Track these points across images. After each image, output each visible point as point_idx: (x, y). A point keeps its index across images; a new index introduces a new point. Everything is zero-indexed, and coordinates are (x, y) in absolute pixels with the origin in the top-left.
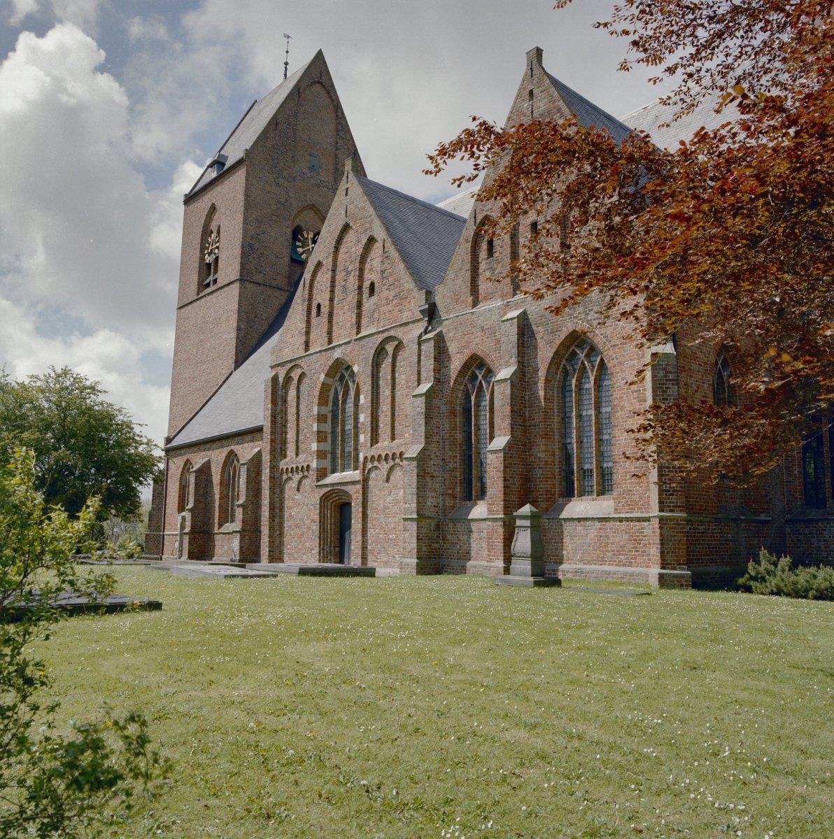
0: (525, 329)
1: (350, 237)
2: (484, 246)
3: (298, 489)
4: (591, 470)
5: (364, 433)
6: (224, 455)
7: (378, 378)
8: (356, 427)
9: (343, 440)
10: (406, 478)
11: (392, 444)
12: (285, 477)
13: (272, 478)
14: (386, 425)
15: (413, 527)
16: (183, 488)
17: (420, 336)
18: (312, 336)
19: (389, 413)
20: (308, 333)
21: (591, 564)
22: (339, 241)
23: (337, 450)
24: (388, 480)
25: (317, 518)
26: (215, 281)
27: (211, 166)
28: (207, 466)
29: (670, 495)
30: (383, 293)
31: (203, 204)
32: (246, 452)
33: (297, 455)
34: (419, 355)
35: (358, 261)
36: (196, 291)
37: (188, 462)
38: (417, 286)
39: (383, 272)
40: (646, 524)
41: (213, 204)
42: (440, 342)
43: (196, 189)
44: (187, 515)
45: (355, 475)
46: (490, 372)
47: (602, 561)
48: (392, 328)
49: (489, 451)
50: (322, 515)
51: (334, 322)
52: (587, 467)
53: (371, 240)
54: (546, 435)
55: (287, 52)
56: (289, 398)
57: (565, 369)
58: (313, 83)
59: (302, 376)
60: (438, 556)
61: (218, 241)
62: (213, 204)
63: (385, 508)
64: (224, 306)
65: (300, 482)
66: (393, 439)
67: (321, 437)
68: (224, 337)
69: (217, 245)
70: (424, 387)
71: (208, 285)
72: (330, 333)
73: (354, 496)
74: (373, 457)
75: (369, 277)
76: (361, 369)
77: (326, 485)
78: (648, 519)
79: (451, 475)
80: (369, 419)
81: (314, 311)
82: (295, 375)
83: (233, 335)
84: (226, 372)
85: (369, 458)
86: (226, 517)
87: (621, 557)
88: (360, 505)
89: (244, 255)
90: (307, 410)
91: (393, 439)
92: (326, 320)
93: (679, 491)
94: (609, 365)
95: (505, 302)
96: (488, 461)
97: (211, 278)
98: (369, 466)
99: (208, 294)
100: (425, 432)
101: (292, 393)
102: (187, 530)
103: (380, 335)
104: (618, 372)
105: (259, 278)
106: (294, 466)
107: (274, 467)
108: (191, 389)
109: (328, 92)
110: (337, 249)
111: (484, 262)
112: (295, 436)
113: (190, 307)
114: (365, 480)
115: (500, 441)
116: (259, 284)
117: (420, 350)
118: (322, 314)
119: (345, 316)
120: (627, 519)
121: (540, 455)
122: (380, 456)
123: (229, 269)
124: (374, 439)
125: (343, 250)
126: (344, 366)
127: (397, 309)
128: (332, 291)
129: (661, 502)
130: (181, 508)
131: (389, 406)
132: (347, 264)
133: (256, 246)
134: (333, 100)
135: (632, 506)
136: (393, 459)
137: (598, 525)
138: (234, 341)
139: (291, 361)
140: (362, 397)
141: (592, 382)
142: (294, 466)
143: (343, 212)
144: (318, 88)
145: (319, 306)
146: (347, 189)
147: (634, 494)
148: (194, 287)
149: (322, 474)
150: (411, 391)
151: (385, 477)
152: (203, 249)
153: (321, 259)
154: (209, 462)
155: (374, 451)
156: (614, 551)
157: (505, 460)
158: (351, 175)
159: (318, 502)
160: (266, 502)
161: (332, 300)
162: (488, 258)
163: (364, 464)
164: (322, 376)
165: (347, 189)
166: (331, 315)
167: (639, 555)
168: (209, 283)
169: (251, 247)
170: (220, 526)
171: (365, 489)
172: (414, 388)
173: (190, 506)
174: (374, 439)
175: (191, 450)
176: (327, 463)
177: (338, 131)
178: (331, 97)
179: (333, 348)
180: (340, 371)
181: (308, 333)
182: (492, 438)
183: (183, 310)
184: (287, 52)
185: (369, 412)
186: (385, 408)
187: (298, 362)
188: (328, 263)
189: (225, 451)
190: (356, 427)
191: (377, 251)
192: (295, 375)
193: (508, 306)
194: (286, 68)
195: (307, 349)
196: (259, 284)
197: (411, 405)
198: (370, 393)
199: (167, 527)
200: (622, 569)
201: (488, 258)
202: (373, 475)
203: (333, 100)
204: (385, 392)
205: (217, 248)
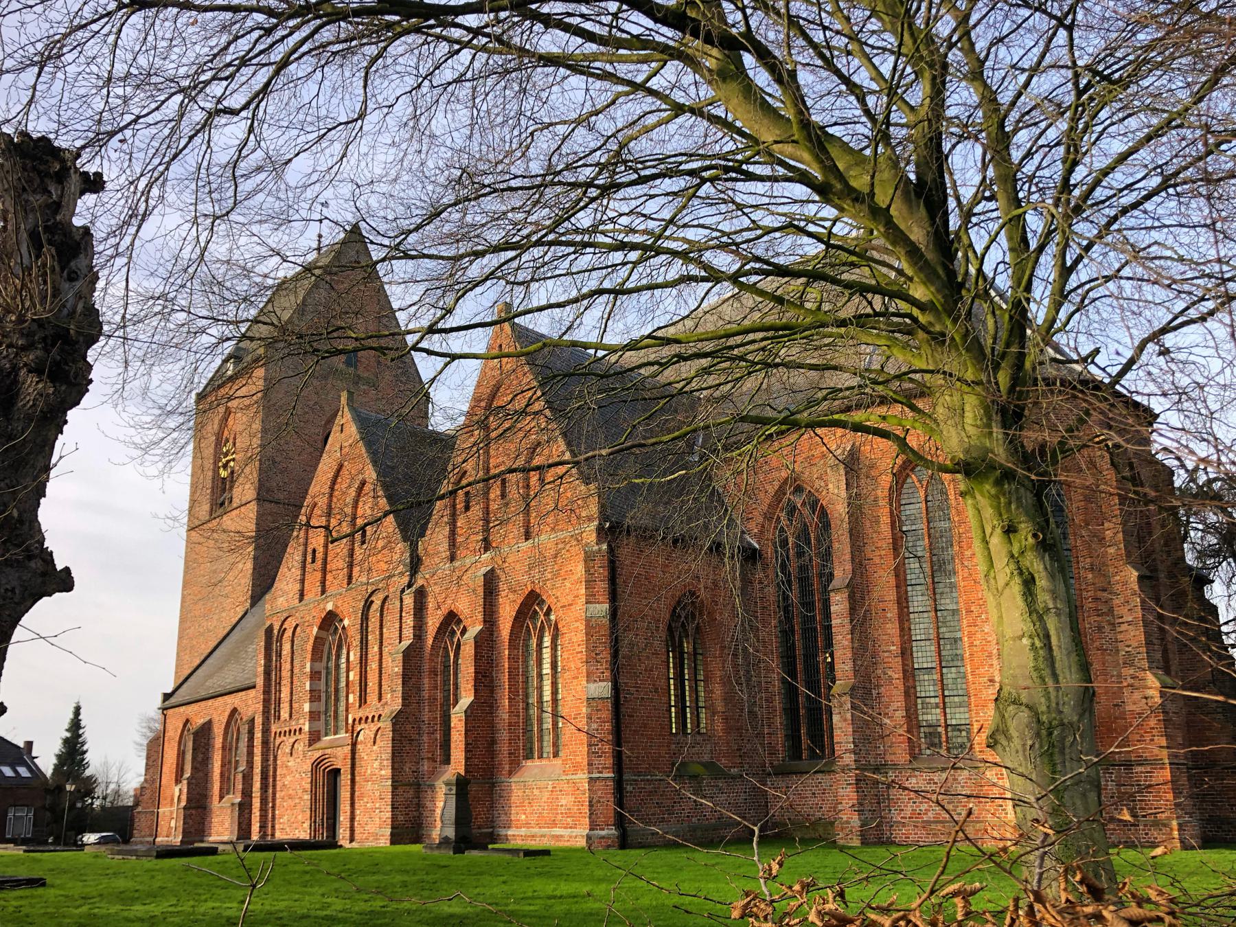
16: (181, 755)
20: (303, 581)
23: (326, 711)
25: (309, 786)
34: (401, 611)
47: (554, 824)
50: (314, 783)
56: (284, 653)
64: (243, 518)
67: (314, 696)
70: (406, 643)
72: (323, 582)
76: (349, 622)
80: (358, 678)
81: (309, 559)
82: (290, 625)
102: (183, 804)
107: (266, 731)
124: (363, 700)
130: (178, 781)
140: (351, 654)
145: (314, 551)
155: (361, 714)
160: (257, 770)
164: (315, 629)
173: (187, 775)
174: (363, 700)
180: (330, 621)
181: (303, 581)
186: (373, 665)
192: (290, 625)
202: (361, 738)
204: (374, 649)
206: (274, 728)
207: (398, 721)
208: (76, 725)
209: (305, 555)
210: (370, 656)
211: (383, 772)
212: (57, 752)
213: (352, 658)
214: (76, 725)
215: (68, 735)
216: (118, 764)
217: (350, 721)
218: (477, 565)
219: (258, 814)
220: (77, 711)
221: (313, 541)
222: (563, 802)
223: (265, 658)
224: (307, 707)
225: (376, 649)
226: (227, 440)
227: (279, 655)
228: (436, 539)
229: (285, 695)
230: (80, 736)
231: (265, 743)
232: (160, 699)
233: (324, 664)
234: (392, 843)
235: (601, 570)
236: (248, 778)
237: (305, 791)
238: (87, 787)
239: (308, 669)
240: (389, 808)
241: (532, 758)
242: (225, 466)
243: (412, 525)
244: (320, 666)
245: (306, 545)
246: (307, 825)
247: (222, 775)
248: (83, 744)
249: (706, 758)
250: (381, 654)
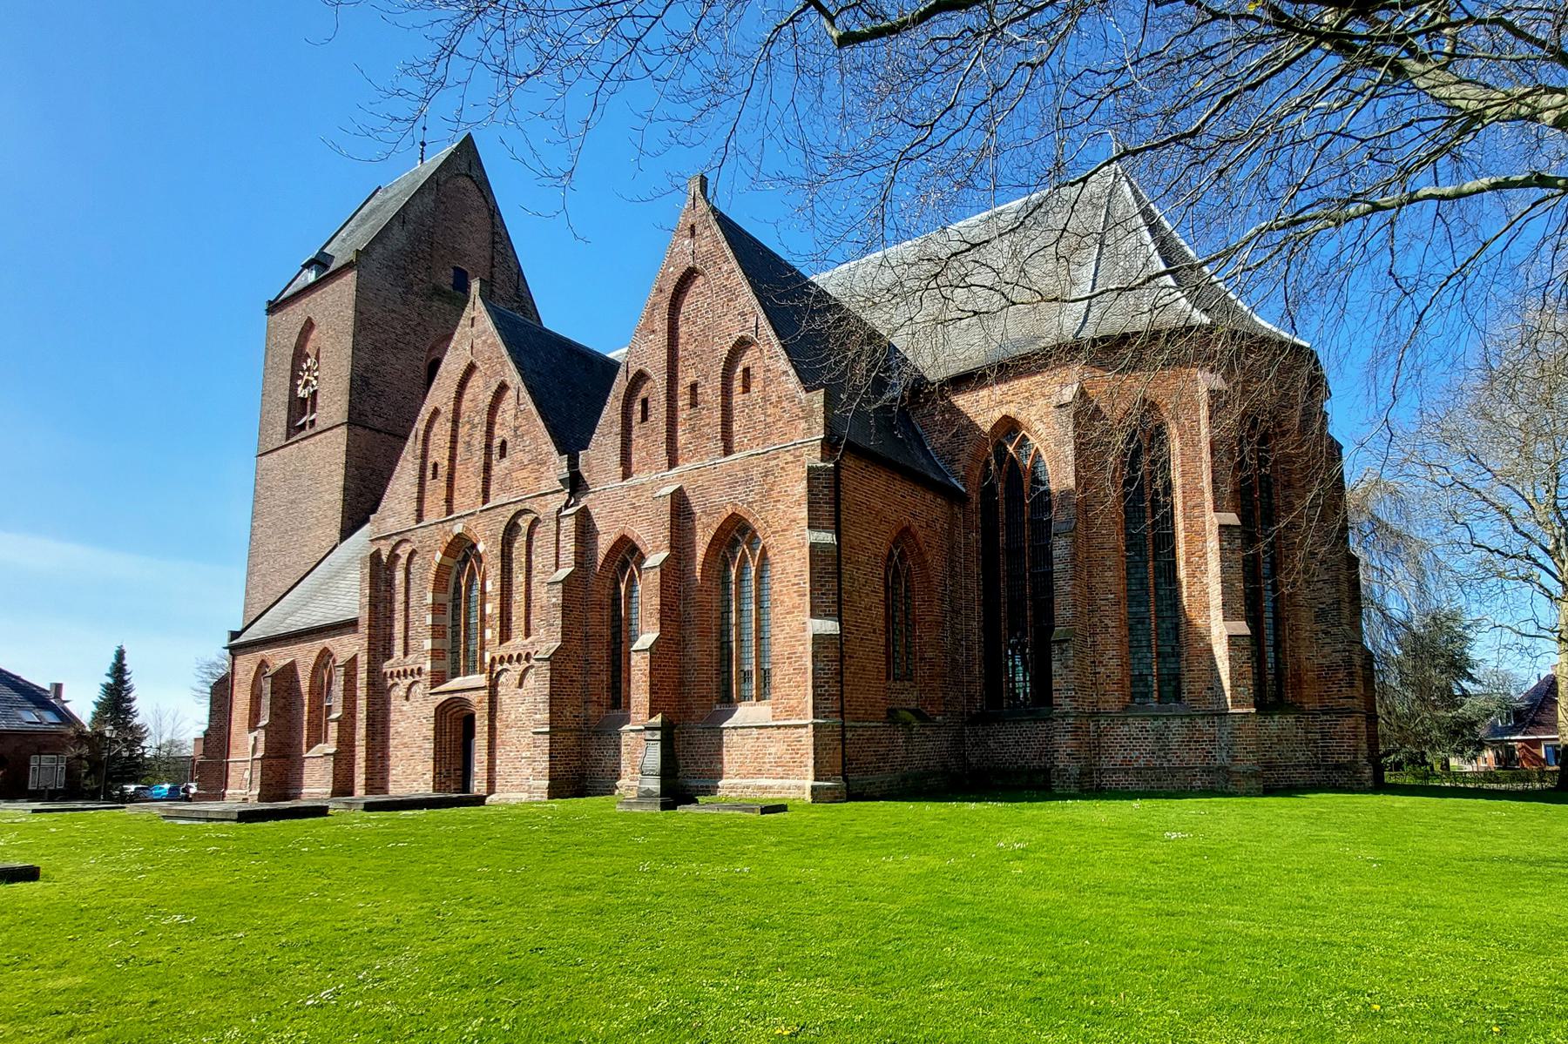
0: (680, 507)
1: (476, 381)
2: (638, 407)
3: (407, 698)
7: (511, 560)
8: (483, 619)
9: (467, 636)
12: (390, 682)
13: (371, 684)
15: (545, 742)
17: (560, 511)
22: (462, 385)
23: (454, 651)
24: (520, 685)
26: (313, 422)
27: (307, 266)
30: (516, 455)
31: (294, 317)
33: (406, 654)
34: (558, 534)
37: (263, 664)
39: (516, 429)
43: (286, 294)
44: (261, 735)
45: (480, 679)
46: (642, 558)
47: (759, 773)
52: (746, 668)
54: (703, 633)
57: (724, 556)
59: (413, 553)
60: (578, 772)
63: (517, 720)
64: (326, 455)
65: (409, 689)
66: (527, 635)
68: (327, 497)
70: (563, 573)
71: (303, 427)
72: (449, 501)
80: (498, 611)
81: (429, 473)
82: (404, 551)
86: (317, 737)
91: (527, 635)
92: (444, 484)
98: (498, 668)
101: (399, 576)
102: (259, 754)
105: (378, 423)
107: (374, 670)
116: (379, 431)
119: (469, 482)
121: (697, 656)
122: (511, 657)
123: (333, 406)
124: (505, 635)
125: (468, 395)
128: (453, 448)
129: (815, 707)
130: (253, 727)
135: (790, 712)
140: (489, 583)
144: (464, 182)
145: (435, 466)
148: (281, 429)
149: (438, 678)
152: (294, 377)
154: (293, 664)
158: (479, 302)
161: (452, 459)
163: (492, 666)
164: (439, 556)
169: (366, 381)
170: (309, 748)
174: (505, 635)
176: (446, 664)
180: (462, 551)
185: (498, 601)
186: (518, 597)
188: (447, 411)
190: (483, 619)
192: (404, 551)
195: (420, 518)
196: (379, 431)
197: (547, 597)
199: (232, 751)
200: (779, 782)
202: (502, 679)
204: (519, 578)
208: (119, 670)
212: (97, 699)
213: (489, 588)
214: (119, 670)
215: (110, 681)
216: (172, 715)
217: (488, 659)
218: (657, 482)
220: (120, 655)
221: (435, 454)
222: (773, 750)
224: (428, 644)
228: (601, 452)
230: (125, 682)
232: (227, 636)
234: (555, 791)
235: (826, 491)
236: (346, 724)
237: (426, 738)
238: (135, 736)
239: (429, 600)
240: (546, 758)
243: (570, 433)
244: (443, 598)
248: (129, 690)
249: (913, 705)
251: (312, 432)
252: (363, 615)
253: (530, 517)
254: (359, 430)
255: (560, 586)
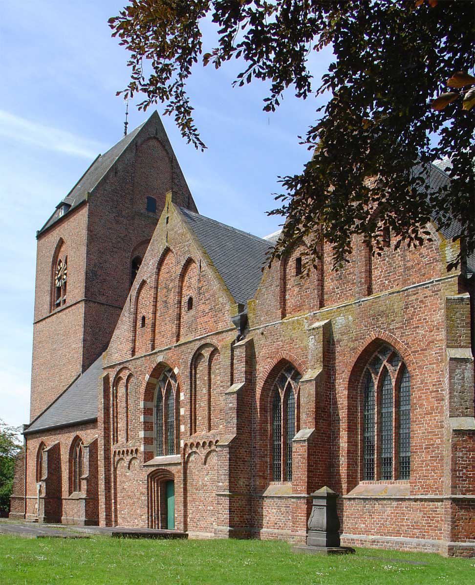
1: (170, 259)
3: (129, 468)
4: (391, 459)
5: (184, 424)
6: (71, 439)
10: (220, 463)
11: (209, 434)
14: (203, 418)
15: (226, 502)
17: (234, 343)
18: (137, 344)
19: (207, 408)
21: (387, 536)
25: (145, 491)
27: (59, 207)
28: (57, 448)
29: (462, 481)
30: (200, 306)
31: (53, 238)
32: (88, 436)
34: (232, 359)
35: (177, 280)
36: (49, 309)
37: (42, 444)
38: (230, 300)
39: (200, 288)
40: (439, 504)
41: (61, 239)
42: (250, 345)
45: (176, 458)
46: (297, 376)
47: (398, 534)
48: (208, 336)
49: (294, 441)
51: (157, 331)
53: (190, 261)
55: (127, 114)
56: (119, 394)
58: (149, 139)
61: (66, 269)
62: (61, 239)
64: (74, 319)
65: (130, 462)
66: (210, 430)
67: (147, 426)
69: (65, 272)
70: (237, 386)
71: (59, 305)
72: (153, 340)
73: (176, 475)
74: (192, 445)
75: (187, 293)
77: (153, 466)
78: (441, 500)
79: (252, 463)
82: (124, 375)
83: (81, 345)
84: (74, 375)
85: (189, 444)
86: (74, 486)
87: (416, 530)
88: (182, 481)
89: (87, 279)
90: (133, 404)
93: (471, 477)
94: (409, 369)
95: (312, 314)
96: (294, 450)
97: (61, 299)
99: (59, 312)
100: (237, 424)
101: (121, 391)
102: (43, 495)
103: (197, 342)
104: (418, 375)
105: (102, 299)
106: (125, 450)
107: (107, 450)
108: (47, 387)
109: (164, 147)
110: (159, 269)
111: (292, 279)
112: (125, 425)
113: (44, 322)
114: (186, 463)
115: (306, 432)
116: (103, 304)
117: (232, 356)
118: (146, 325)
119: (166, 328)
120: (421, 500)
122: (198, 444)
123: (76, 290)
124: (193, 429)
126: (167, 369)
127: (214, 320)
128: (155, 306)
130: (39, 478)
131: (206, 403)
132: (168, 282)
133: (99, 273)
134: (168, 153)
136: (210, 445)
137: (395, 504)
138: (81, 350)
139: (120, 364)
140: (182, 394)
141: (394, 384)
142: (125, 450)
143: (164, 238)
145: (144, 318)
146: (168, 218)
147: (429, 479)
148: (47, 306)
150: (223, 390)
151: (203, 460)
152: (53, 275)
153: (145, 279)
154: (59, 444)
156: (409, 525)
157: (308, 449)
159: (146, 478)
160: (102, 476)
161: (155, 313)
162: (297, 275)
163: (184, 449)
164: (147, 377)
165: (168, 218)
166: (154, 325)
167: (431, 530)
168: (60, 303)
169: (95, 273)
171: (185, 469)
172: (228, 387)
173: (45, 477)
174: (193, 429)
175: (58, 432)
177: (173, 178)
178: (166, 150)
179: (156, 353)
180: (162, 372)
181: (134, 341)
182: (298, 429)
183: (38, 325)
184: (127, 114)
186: (202, 404)
187: (127, 365)
188: (151, 282)
189: (72, 435)
191: (194, 269)
192: (124, 375)
193: (315, 318)
194: (126, 127)
196: (103, 304)
198: (188, 391)
201: (297, 275)
202: (192, 458)
203: (168, 153)
204: (202, 391)
205: (66, 274)
206: (113, 448)
207: (233, 447)
209: (135, 322)
210: (198, 397)
211: (221, 484)
217: (182, 445)
219: (104, 506)
221: (143, 311)
223: (104, 398)
225: (205, 391)
226: (60, 261)
227: (116, 397)
229: (121, 425)
231: (107, 458)
233: (155, 402)
236: (92, 480)
241: (373, 479)
242: (59, 279)
244: (150, 405)
245: (136, 314)
246: (145, 517)
247: (70, 479)
250: (210, 395)
251: (64, 307)
252: (100, 416)
253: (127, 373)
254: (92, 304)
255: (235, 395)
